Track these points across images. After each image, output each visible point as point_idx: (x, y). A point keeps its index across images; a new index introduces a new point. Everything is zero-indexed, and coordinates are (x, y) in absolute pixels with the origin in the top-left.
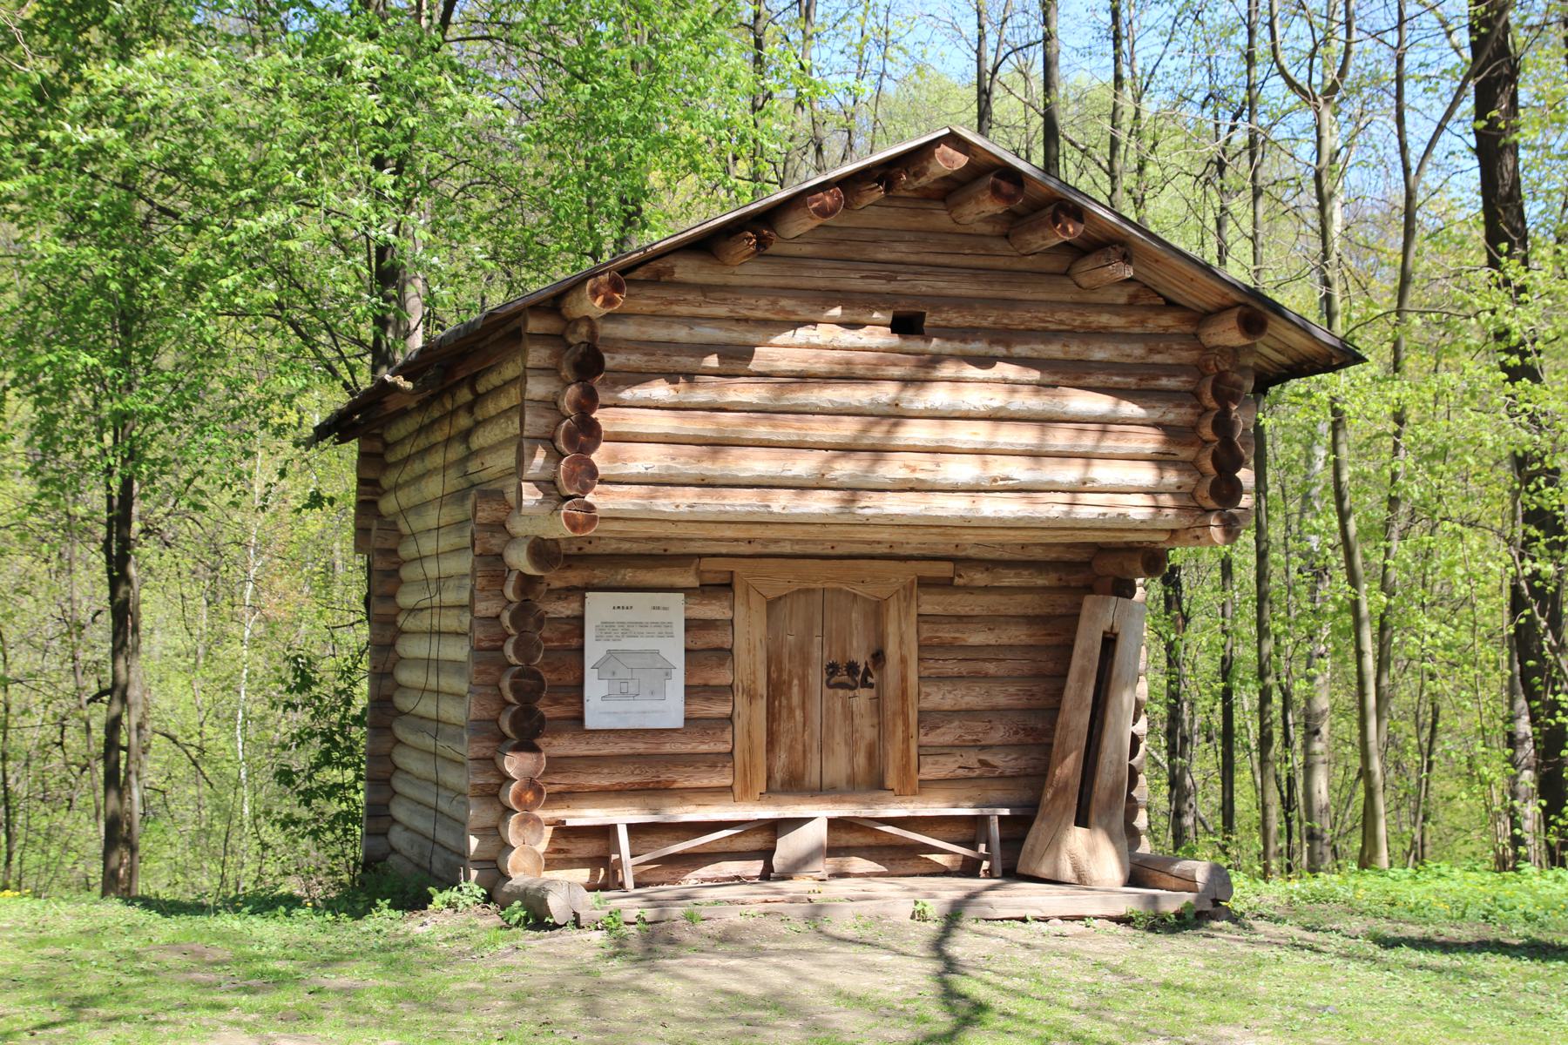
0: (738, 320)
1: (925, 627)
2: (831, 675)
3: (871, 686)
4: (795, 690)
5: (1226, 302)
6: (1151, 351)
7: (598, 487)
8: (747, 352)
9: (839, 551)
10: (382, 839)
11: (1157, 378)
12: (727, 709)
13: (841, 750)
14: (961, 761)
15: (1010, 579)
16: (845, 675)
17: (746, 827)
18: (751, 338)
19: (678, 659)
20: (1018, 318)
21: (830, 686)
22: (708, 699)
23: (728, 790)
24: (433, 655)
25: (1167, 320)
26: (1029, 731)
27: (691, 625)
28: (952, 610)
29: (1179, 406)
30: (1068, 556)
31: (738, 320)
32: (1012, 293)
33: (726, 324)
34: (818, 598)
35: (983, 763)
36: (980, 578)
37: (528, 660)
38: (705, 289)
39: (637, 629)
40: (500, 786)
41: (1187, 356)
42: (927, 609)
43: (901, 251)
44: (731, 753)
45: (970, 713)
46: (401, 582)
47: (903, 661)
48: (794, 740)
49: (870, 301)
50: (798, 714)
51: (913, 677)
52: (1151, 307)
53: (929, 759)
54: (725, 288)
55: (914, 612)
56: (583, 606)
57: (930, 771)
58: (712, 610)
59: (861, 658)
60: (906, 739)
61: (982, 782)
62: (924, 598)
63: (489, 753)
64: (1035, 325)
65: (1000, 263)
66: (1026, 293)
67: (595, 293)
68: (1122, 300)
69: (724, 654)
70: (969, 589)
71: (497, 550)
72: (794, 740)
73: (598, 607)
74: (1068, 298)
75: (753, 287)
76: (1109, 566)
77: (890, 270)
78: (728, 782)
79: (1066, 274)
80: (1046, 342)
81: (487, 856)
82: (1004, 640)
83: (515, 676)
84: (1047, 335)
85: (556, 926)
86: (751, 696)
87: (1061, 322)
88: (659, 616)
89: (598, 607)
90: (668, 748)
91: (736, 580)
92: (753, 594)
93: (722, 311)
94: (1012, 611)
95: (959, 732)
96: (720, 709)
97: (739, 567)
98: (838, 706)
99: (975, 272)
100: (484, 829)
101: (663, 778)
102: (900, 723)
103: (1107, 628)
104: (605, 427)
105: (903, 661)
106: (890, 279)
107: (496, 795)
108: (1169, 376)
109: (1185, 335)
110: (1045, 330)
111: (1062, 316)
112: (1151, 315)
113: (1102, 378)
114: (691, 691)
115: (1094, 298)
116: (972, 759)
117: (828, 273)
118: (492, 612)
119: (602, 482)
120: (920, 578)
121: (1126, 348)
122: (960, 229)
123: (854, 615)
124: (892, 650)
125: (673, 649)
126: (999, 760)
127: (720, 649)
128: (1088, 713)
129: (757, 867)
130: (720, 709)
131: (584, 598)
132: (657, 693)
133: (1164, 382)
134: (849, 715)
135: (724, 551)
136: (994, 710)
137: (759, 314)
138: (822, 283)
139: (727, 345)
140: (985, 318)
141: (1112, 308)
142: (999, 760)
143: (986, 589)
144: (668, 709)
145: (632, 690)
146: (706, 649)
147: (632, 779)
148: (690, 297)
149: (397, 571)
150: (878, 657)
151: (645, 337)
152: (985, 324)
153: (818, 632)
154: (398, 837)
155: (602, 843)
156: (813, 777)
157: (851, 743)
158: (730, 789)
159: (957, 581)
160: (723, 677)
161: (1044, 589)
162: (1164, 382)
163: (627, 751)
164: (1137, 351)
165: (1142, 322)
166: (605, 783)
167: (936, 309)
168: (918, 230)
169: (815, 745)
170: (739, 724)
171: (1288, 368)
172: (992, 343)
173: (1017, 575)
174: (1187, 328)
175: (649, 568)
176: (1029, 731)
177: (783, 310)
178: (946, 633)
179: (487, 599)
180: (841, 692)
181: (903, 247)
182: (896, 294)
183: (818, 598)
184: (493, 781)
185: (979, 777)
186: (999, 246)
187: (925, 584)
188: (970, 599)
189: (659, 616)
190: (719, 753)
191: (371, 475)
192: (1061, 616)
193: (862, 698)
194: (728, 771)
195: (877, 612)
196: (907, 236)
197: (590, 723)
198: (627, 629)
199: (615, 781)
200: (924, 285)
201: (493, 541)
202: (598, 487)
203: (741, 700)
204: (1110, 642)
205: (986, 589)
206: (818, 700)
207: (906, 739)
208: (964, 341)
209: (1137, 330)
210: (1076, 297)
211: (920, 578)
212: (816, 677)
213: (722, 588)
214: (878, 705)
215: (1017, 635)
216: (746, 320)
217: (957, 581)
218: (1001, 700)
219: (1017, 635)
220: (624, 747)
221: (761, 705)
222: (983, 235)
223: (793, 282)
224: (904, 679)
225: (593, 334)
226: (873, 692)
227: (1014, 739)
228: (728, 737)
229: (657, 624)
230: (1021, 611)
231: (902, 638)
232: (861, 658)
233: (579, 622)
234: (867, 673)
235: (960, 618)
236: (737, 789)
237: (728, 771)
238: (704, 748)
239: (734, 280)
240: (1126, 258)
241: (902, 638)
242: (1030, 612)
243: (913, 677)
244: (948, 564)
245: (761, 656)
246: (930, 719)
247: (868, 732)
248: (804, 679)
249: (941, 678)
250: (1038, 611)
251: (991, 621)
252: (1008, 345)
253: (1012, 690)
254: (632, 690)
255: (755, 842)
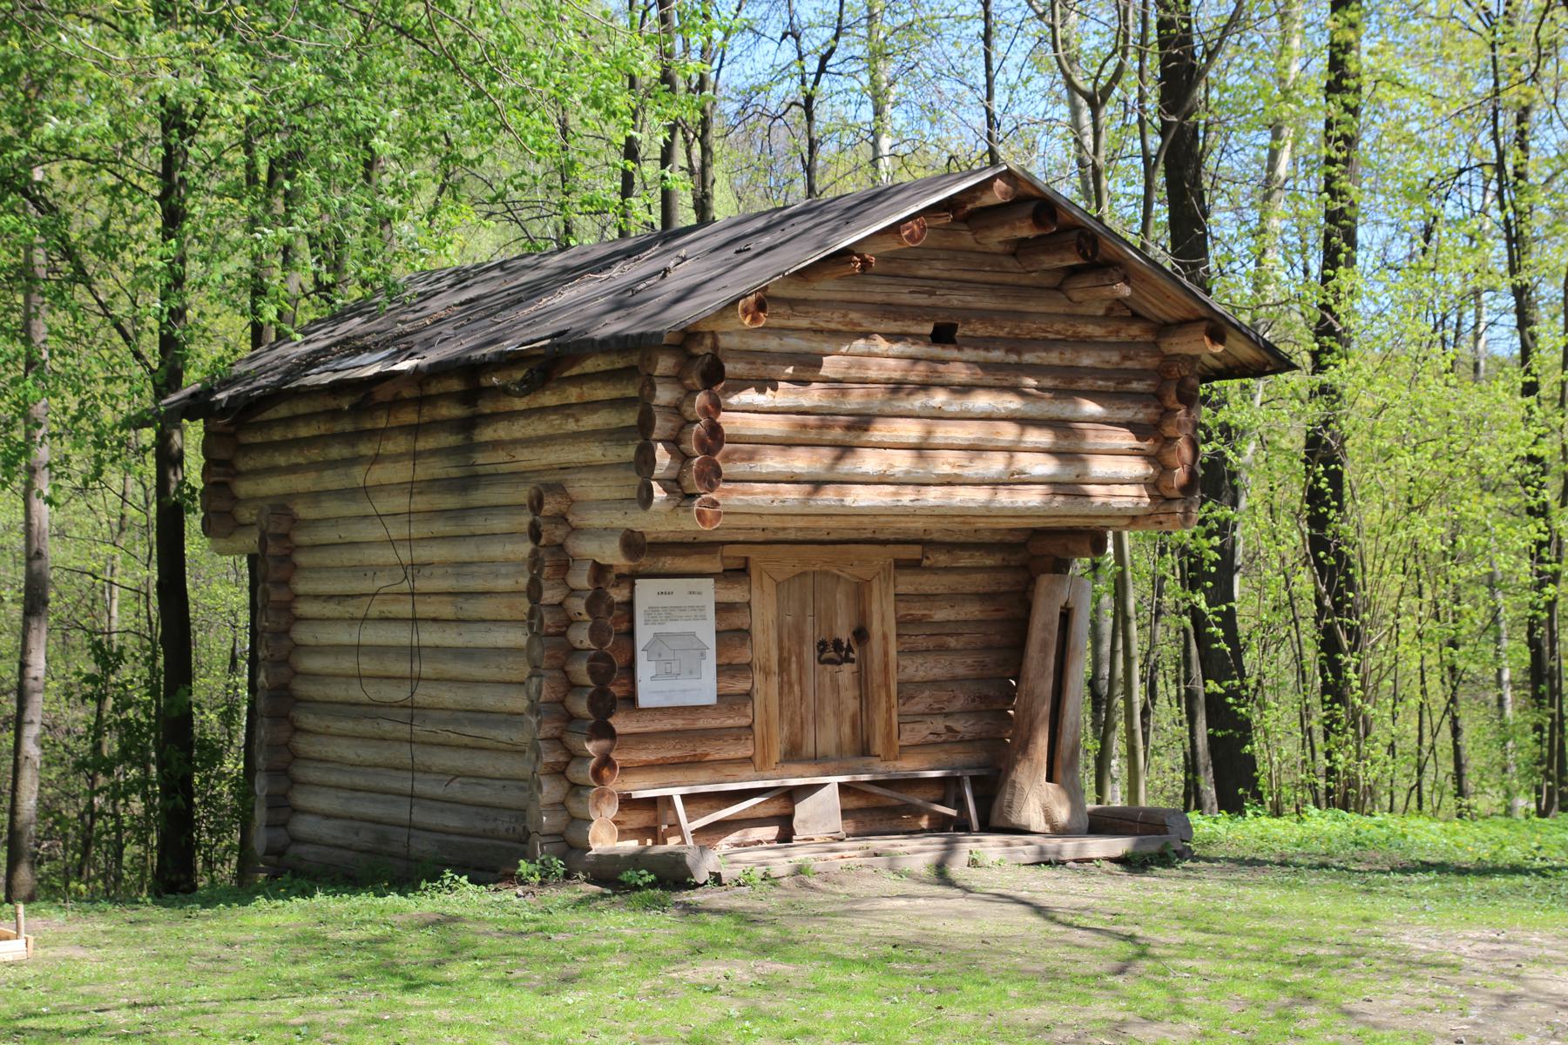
0: (815, 331)
1: (902, 605)
2: (822, 651)
3: (852, 661)
4: (794, 666)
5: (1191, 317)
6: (1125, 358)
7: (722, 486)
8: (814, 362)
9: (833, 537)
10: (282, 831)
11: (1129, 382)
12: (748, 686)
13: (830, 721)
14: (932, 728)
15: (966, 560)
16: (833, 652)
17: (772, 794)
18: (826, 347)
19: (711, 641)
20: (1030, 328)
21: (821, 662)
22: (733, 677)
23: (749, 760)
24: (415, 643)
25: (1135, 330)
26: (983, 698)
27: (722, 608)
28: (927, 589)
29: (1147, 406)
30: (1009, 538)
31: (815, 331)
32: (1021, 307)
33: (808, 335)
34: (809, 580)
35: (949, 729)
36: (942, 559)
37: (602, 644)
38: (528, 413)
39: (677, 613)
40: (567, 764)
41: (1151, 362)
42: (902, 589)
43: (938, 269)
44: (750, 727)
45: (934, 683)
46: (295, 566)
47: (885, 637)
48: (794, 712)
49: (916, 313)
50: (796, 688)
51: (893, 653)
52: (1122, 319)
53: (908, 727)
54: (805, 302)
55: (892, 592)
56: (632, 592)
57: (907, 738)
58: (735, 594)
59: (844, 634)
60: (889, 710)
61: (947, 746)
62: (901, 579)
63: (557, 733)
64: (1039, 334)
65: (1010, 279)
66: (1031, 306)
67: (746, 312)
68: (1101, 312)
69: (744, 634)
70: (933, 570)
71: (559, 540)
72: (794, 712)
73: (646, 592)
74: (1061, 310)
75: (826, 301)
76: (1053, 548)
77: (931, 285)
78: (750, 753)
79: (1058, 288)
80: (1047, 350)
81: (555, 830)
82: (962, 617)
83: (592, 660)
84: (1048, 344)
85: (697, 885)
86: (767, 673)
87: (1058, 332)
88: (694, 600)
89: (646, 592)
90: (703, 723)
91: (752, 565)
92: (765, 578)
93: (804, 323)
94: (968, 589)
95: (930, 701)
96: (741, 686)
97: (754, 554)
98: (827, 680)
99: (993, 287)
100: (552, 805)
101: (699, 751)
102: (883, 695)
103: (1062, 603)
104: (727, 430)
105: (885, 637)
106: (932, 294)
107: (563, 773)
108: (1139, 380)
109: (1146, 343)
110: (1045, 339)
111: (1058, 326)
112: (1123, 325)
113: (1090, 382)
114: (724, 669)
115: (1081, 310)
116: (939, 724)
117: (886, 289)
118: (556, 600)
119: (726, 481)
120: (896, 561)
121: (1106, 355)
122: (980, 248)
123: (838, 596)
124: (876, 628)
125: (706, 632)
126: (960, 725)
127: (739, 630)
128: (1051, 681)
129: (772, 832)
130: (741, 686)
131: (633, 585)
132: (694, 673)
133: (1135, 386)
134: (836, 689)
135: (741, 538)
136: (954, 679)
137: (833, 326)
138: (879, 298)
139: (807, 353)
140: (1002, 328)
141: (1092, 319)
142: (960, 725)
143: (948, 570)
144: (703, 687)
145: (675, 670)
146: (732, 634)
147: (674, 753)
148: (781, 311)
149: (288, 556)
150: (861, 634)
151: (745, 347)
152: (1001, 334)
153: (809, 612)
154: (304, 826)
155: (652, 814)
156: (809, 748)
157: (838, 714)
158: (749, 760)
159: (926, 562)
160: (742, 656)
161: (992, 568)
162: (1135, 386)
163: (669, 727)
164: (1115, 357)
165: (1118, 332)
166: (652, 758)
167: (967, 322)
168: (948, 249)
169: (810, 717)
170: (758, 698)
171: (1214, 369)
172: (1008, 351)
173: (971, 557)
174: (1150, 338)
175: (684, 556)
176: (983, 698)
177: (852, 323)
178: (918, 611)
179: (552, 588)
180: (829, 667)
181: (939, 265)
182: (934, 307)
183: (809, 580)
184: (562, 759)
185: (944, 742)
186: (1010, 263)
187: (901, 565)
188: (935, 578)
189: (694, 600)
190: (740, 728)
191: (223, 454)
192: (1003, 593)
193: (846, 672)
194: (750, 742)
195: (860, 591)
196: (942, 255)
197: (644, 700)
198: (670, 613)
199: (660, 756)
200: (956, 299)
201: (558, 533)
202: (722, 486)
203: (758, 677)
204: (1066, 616)
205: (948, 570)
206: (816, 675)
207: (889, 710)
208: (987, 349)
209: (1113, 339)
210: (1068, 310)
211: (896, 561)
212: (810, 653)
213: (738, 573)
214: (862, 680)
215: (972, 611)
216: (821, 331)
217: (926, 562)
218: (961, 671)
219: (972, 611)
220: (666, 724)
221: (775, 679)
222: (995, 254)
223: (857, 297)
224: (886, 654)
225: (715, 346)
226: (854, 667)
227: (971, 706)
228: (749, 711)
229: (693, 608)
230: (973, 589)
231: (883, 618)
232: (844, 634)
233: (630, 605)
234: (849, 649)
235: (927, 596)
236: (758, 759)
237: (750, 742)
238: (730, 722)
239: (814, 295)
240: (1126, 280)
241: (883, 618)
242: (981, 590)
243: (893, 653)
244: (915, 548)
245: (773, 634)
246: (908, 689)
247: (851, 704)
248: (800, 655)
249: (913, 652)
250: (987, 589)
251: (954, 597)
252: (1019, 353)
253: (969, 661)
254: (675, 670)
255: (774, 809)
